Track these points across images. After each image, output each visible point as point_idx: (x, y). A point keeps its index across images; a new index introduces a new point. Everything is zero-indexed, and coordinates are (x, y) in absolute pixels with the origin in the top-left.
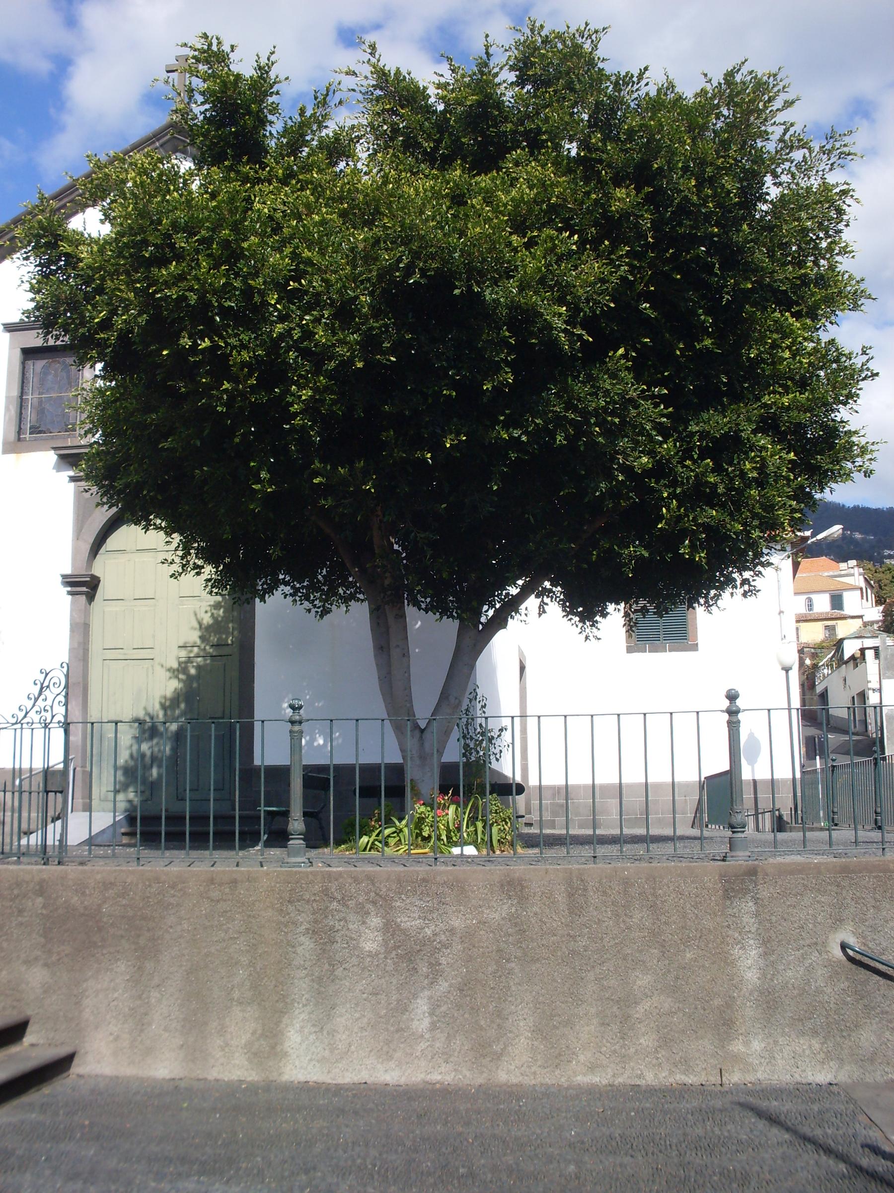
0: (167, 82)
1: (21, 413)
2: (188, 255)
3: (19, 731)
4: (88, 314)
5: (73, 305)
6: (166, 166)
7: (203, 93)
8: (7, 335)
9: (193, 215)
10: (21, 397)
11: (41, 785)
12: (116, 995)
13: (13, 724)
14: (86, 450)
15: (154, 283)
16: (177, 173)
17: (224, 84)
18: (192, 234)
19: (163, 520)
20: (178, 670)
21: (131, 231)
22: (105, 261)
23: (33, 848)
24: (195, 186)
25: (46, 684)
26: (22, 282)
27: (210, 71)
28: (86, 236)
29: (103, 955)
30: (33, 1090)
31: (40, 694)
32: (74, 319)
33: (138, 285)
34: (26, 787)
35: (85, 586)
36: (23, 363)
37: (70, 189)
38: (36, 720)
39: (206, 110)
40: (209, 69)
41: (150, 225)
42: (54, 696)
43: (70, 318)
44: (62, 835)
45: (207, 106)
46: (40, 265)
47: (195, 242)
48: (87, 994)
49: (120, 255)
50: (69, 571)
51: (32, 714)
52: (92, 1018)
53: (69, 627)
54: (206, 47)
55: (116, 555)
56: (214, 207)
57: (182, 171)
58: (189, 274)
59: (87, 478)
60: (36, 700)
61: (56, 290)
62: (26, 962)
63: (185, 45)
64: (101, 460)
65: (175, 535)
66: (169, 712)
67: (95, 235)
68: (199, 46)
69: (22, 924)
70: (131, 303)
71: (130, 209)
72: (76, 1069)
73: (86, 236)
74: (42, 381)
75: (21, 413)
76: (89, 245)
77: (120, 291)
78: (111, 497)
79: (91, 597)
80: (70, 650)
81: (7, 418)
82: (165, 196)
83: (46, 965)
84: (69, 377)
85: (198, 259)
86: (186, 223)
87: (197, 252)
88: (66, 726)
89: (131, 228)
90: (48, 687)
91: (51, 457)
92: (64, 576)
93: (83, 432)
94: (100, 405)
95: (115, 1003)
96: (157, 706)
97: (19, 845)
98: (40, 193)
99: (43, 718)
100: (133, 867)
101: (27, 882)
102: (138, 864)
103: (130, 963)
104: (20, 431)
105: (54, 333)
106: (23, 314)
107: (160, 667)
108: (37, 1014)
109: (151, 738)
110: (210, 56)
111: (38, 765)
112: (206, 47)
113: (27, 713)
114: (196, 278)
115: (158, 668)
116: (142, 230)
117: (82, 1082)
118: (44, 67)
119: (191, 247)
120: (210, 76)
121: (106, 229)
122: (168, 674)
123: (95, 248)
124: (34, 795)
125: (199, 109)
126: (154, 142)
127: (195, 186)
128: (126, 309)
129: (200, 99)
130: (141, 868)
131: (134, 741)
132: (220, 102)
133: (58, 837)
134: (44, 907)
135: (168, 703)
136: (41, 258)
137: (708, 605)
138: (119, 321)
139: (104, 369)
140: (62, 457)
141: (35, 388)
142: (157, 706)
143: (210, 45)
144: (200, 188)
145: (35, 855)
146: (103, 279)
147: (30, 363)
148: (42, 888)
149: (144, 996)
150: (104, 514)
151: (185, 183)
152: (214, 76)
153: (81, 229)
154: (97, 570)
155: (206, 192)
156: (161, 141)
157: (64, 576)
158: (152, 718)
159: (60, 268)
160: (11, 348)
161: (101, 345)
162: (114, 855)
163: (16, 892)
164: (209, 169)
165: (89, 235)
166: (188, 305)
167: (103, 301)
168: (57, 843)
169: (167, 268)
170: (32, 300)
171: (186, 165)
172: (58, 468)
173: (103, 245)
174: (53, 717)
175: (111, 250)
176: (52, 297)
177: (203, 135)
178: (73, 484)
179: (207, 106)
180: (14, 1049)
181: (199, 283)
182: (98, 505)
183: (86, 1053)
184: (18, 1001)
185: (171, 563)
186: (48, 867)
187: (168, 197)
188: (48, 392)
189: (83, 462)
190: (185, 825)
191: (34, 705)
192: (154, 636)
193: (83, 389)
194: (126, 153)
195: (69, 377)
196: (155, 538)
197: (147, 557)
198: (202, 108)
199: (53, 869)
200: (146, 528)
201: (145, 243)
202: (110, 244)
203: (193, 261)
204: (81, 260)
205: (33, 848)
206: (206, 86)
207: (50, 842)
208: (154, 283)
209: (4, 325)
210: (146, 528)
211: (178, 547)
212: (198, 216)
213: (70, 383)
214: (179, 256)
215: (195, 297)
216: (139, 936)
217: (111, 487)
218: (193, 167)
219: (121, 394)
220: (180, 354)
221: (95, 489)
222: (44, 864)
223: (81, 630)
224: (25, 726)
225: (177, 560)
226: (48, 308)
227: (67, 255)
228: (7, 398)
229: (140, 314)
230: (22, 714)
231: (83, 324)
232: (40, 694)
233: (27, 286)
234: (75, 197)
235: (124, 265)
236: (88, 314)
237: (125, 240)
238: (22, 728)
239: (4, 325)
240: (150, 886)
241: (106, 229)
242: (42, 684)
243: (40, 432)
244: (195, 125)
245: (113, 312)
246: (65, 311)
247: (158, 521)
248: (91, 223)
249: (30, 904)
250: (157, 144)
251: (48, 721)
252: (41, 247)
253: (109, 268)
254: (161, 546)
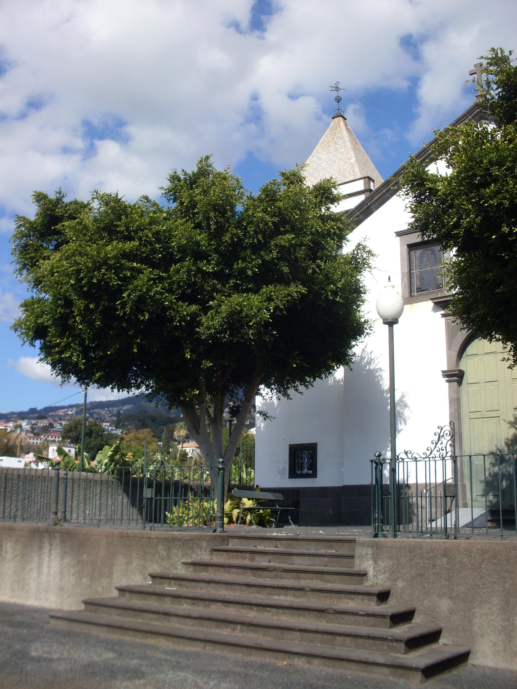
0: (474, 81)
1: (411, 281)
2: (501, 178)
3: (428, 462)
4: (445, 221)
5: (438, 217)
6: (480, 129)
7: (496, 83)
8: (398, 238)
9: (500, 155)
10: (410, 272)
11: (442, 493)
12: (493, 618)
13: (424, 458)
14: (452, 298)
15: (482, 198)
16: (487, 132)
17: (508, 75)
18: (501, 166)
19: (500, 335)
20: (514, 423)
21: (466, 170)
22: (453, 189)
23: (439, 529)
24: (499, 138)
25: (442, 434)
26: (407, 208)
27: (499, 69)
28: (439, 176)
29: (484, 593)
30: (447, 671)
31: (439, 440)
32: (438, 225)
33: (474, 200)
34: (433, 495)
35: (455, 377)
36: (409, 253)
37: (424, 151)
38: (437, 455)
39: (499, 92)
40: (498, 68)
41: (476, 165)
42: (446, 440)
43: (435, 224)
44: (456, 522)
45: (500, 90)
46: (415, 197)
47: (504, 170)
48: (475, 616)
49: (461, 185)
50: (446, 369)
51: (435, 452)
52: (479, 631)
53: (448, 401)
54: (494, 56)
55: (473, 357)
56: (513, 148)
57: (489, 130)
58: (503, 189)
59: (454, 315)
60: (436, 444)
61: (426, 209)
62: (439, 596)
63: (482, 57)
64: (460, 303)
65: (508, 343)
66: (511, 448)
67: (444, 175)
68: (490, 56)
69: (435, 573)
70: (471, 211)
71: (464, 158)
72: (472, 661)
73: (439, 176)
74: (421, 262)
75: (411, 281)
76: (442, 181)
77: (464, 205)
78: (469, 324)
79: (460, 383)
80: (450, 414)
81: (403, 284)
82: (482, 146)
83: (451, 598)
84: (435, 258)
85: (507, 180)
86: (497, 160)
87: (506, 176)
88: (454, 459)
89: (465, 168)
90: (443, 436)
91: (430, 304)
92: (443, 372)
93: (448, 288)
94: (456, 272)
95: (493, 622)
96: (504, 444)
97: (427, 527)
98: (410, 157)
99: (441, 454)
100: (499, 540)
101: (437, 549)
102: (502, 539)
103: (500, 599)
104: (411, 291)
105: (428, 234)
106: (409, 225)
107: (503, 421)
108: (447, 626)
109: (501, 463)
110: (497, 61)
111: (440, 480)
112: (494, 56)
113: (432, 452)
114: (507, 191)
115: (502, 422)
116: (472, 168)
117: (475, 669)
118: (405, 84)
119: (502, 174)
120: (499, 72)
121: (450, 172)
122: (509, 425)
123: (446, 183)
124: (439, 499)
125: (495, 92)
126: (468, 117)
127: (499, 138)
128: (468, 215)
129: (495, 87)
130: (504, 541)
131: (491, 466)
132: (508, 86)
133: (453, 523)
134: (448, 563)
135: (510, 443)
136: (415, 193)
137: (365, 293)
138: (465, 222)
139: (457, 251)
140: (436, 304)
141: (417, 266)
142: (504, 444)
143: (497, 54)
144: (501, 138)
145: (442, 534)
146: (452, 199)
147: (413, 252)
148: (446, 553)
149: (510, 619)
150: (464, 334)
151: (492, 137)
152: (501, 71)
153: (436, 173)
154: (462, 367)
155: (506, 140)
156: (472, 115)
157: (443, 372)
158: (501, 452)
159: (426, 197)
160: (401, 245)
161: (455, 237)
162: (487, 533)
163: (431, 554)
164: (505, 126)
165: (441, 176)
166: (504, 208)
167: (453, 212)
168: (453, 526)
169: (489, 188)
170: (413, 217)
171: (491, 127)
172: (435, 310)
173: (449, 181)
174: (447, 453)
175: (455, 183)
176: (424, 214)
177: (500, 107)
178: (444, 319)
179: (500, 90)
180: (434, 646)
181: (509, 194)
182: (461, 329)
183: (477, 652)
184: (435, 618)
185: (508, 360)
186: (449, 540)
187: (483, 147)
188: (424, 267)
189: (451, 305)
190: (500, 516)
191: (435, 447)
192: (499, 403)
193: (446, 263)
194: (454, 125)
195: (435, 258)
196: (497, 346)
197: (491, 357)
198: (497, 92)
199: (451, 541)
200: (491, 340)
201: (475, 175)
202: (454, 179)
203: (504, 181)
204: (438, 191)
205: (439, 529)
206: (498, 78)
207: (449, 526)
208: (482, 198)
209: (395, 233)
210: (491, 340)
211: (511, 349)
212: (504, 155)
213: (436, 261)
214: (495, 180)
215: (508, 202)
216: (505, 582)
217: (468, 318)
218: (495, 127)
219: (470, 264)
220: (503, 237)
221: (459, 321)
222: (446, 539)
223: (456, 403)
224: (431, 459)
225: (511, 358)
226: (422, 220)
227: (430, 189)
228: (402, 273)
229: (476, 217)
230: (428, 453)
231: (443, 226)
232: (439, 440)
233: (409, 210)
234: (428, 155)
235: (464, 190)
236: (445, 221)
237: (463, 175)
238: (429, 461)
239: (395, 233)
240: (510, 552)
241: (450, 172)
242: (439, 435)
243: (423, 291)
244: (494, 102)
245: (460, 218)
246: (433, 221)
247: (497, 336)
248: (440, 169)
249: (439, 562)
250: (470, 117)
251: (444, 456)
252: (415, 187)
253: (455, 192)
254: (501, 350)
